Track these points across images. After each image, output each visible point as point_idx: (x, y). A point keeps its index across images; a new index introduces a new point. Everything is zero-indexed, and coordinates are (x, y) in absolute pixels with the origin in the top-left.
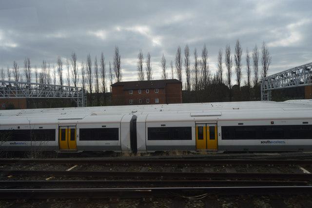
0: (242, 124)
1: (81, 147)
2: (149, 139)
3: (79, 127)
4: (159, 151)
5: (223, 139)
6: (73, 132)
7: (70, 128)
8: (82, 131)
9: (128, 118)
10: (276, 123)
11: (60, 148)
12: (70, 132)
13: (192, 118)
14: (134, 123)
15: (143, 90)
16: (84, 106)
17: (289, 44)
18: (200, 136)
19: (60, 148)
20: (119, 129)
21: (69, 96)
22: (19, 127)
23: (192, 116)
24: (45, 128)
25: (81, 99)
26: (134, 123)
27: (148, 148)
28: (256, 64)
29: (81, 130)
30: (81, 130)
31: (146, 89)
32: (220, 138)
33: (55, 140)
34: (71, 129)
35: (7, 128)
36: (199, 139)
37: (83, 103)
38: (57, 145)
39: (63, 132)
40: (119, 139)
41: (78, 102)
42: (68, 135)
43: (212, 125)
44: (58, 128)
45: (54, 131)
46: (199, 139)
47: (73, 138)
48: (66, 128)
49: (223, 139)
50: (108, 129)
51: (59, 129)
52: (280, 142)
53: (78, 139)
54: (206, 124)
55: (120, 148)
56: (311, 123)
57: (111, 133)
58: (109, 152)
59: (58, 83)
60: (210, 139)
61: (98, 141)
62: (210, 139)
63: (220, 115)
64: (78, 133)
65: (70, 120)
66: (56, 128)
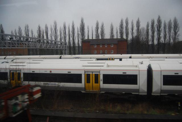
0: (125, 73)
1: (103, 89)
3: (22, 72)
4: (171, 94)
5: (104, 83)
6: (97, 77)
7: (94, 73)
8: (104, 76)
9: (145, 68)
10: (53, 72)
12: (17, 75)
13: (83, 68)
14: (150, 71)
15: (103, 45)
16: (67, 55)
21: (40, 47)
22: (51, 72)
23: (83, 66)
24: (73, 72)
25: (66, 50)
26: (150, 71)
27: (162, 91)
28: (170, 31)
30: (104, 76)
31: (100, 44)
32: (101, 82)
33: (81, 83)
34: (95, 74)
36: (87, 83)
38: (83, 86)
40: (99, 83)
41: (63, 51)
42: (92, 79)
43: (89, 73)
44: (84, 73)
45: (80, 75)
46: (87, 83)
48: (91, 73)
49: (104, 83)
52: (52, 84)
54: (92, 72)
55: (138, 90)
56: (180, 74)
57: (132, 79)
58: (128, 94)
59: (36, 35)
60: (95, 83)
62: (95, 83)
63: (103, 66)
64: (101, 77)
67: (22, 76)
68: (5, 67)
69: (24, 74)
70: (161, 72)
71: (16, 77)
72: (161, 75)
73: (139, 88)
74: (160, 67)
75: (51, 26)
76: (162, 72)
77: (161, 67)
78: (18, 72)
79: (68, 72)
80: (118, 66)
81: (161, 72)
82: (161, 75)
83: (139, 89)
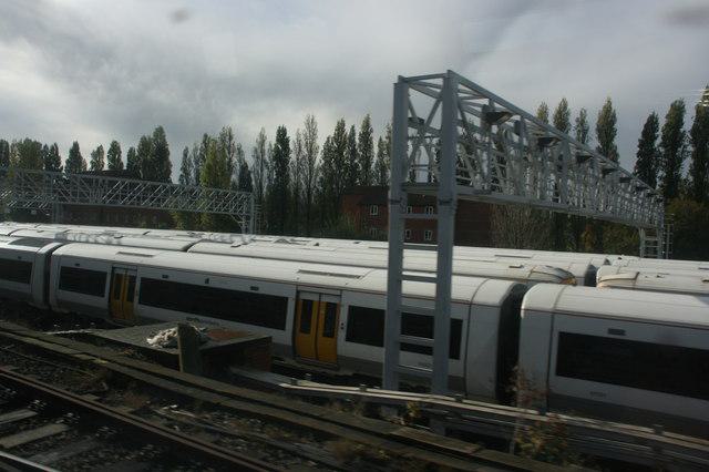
0: (622, 332)
2: (561, 371)
5: (349, 338)
6: (332, 309)
9: (495, 292)
11: (295, 352)
12: (323, 312)
17: (598, 68)
18: (115, 294)
19: (295, 352)
20: (465, 324)
22: (207, 281)
29: (143, 279)
32: (342, 334)
33: (283, 329)
34: (328, 304)
35: (233, 287)
37: (642, 234)
39: (305, 307)
42: (318, 317)
45: (283, 301)
47: (330, 332)
48: (315, 298)
49: (349, 338)
50: (171, 282)
51: (297, 296)
53: (342, 334)
61: (623, 388)
64: (343, 316)
65: (142, 258)
66: (109, 271)
67: (343, 316)
68: (549, 306)
69: (353, 310)
70: (553, 317)
71: (125, 284)
72: (552, 330)
73: (465, 374)
74: (559, 296)
75: (298, 134)
76: (556, 316)
77: (563, 296)
78: (325, 299)
79: (252, 288)
80: (253, 257)
81: (553, 317)
82: (552, 330)
83: (464, 379)
